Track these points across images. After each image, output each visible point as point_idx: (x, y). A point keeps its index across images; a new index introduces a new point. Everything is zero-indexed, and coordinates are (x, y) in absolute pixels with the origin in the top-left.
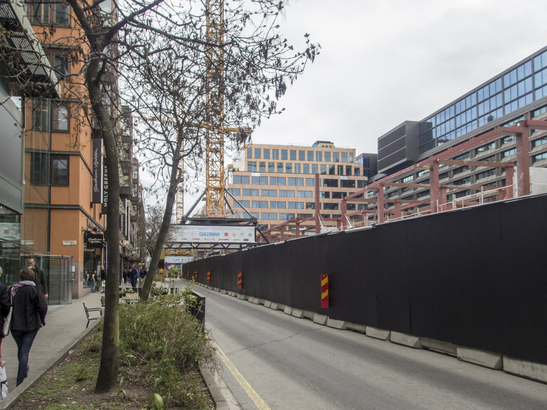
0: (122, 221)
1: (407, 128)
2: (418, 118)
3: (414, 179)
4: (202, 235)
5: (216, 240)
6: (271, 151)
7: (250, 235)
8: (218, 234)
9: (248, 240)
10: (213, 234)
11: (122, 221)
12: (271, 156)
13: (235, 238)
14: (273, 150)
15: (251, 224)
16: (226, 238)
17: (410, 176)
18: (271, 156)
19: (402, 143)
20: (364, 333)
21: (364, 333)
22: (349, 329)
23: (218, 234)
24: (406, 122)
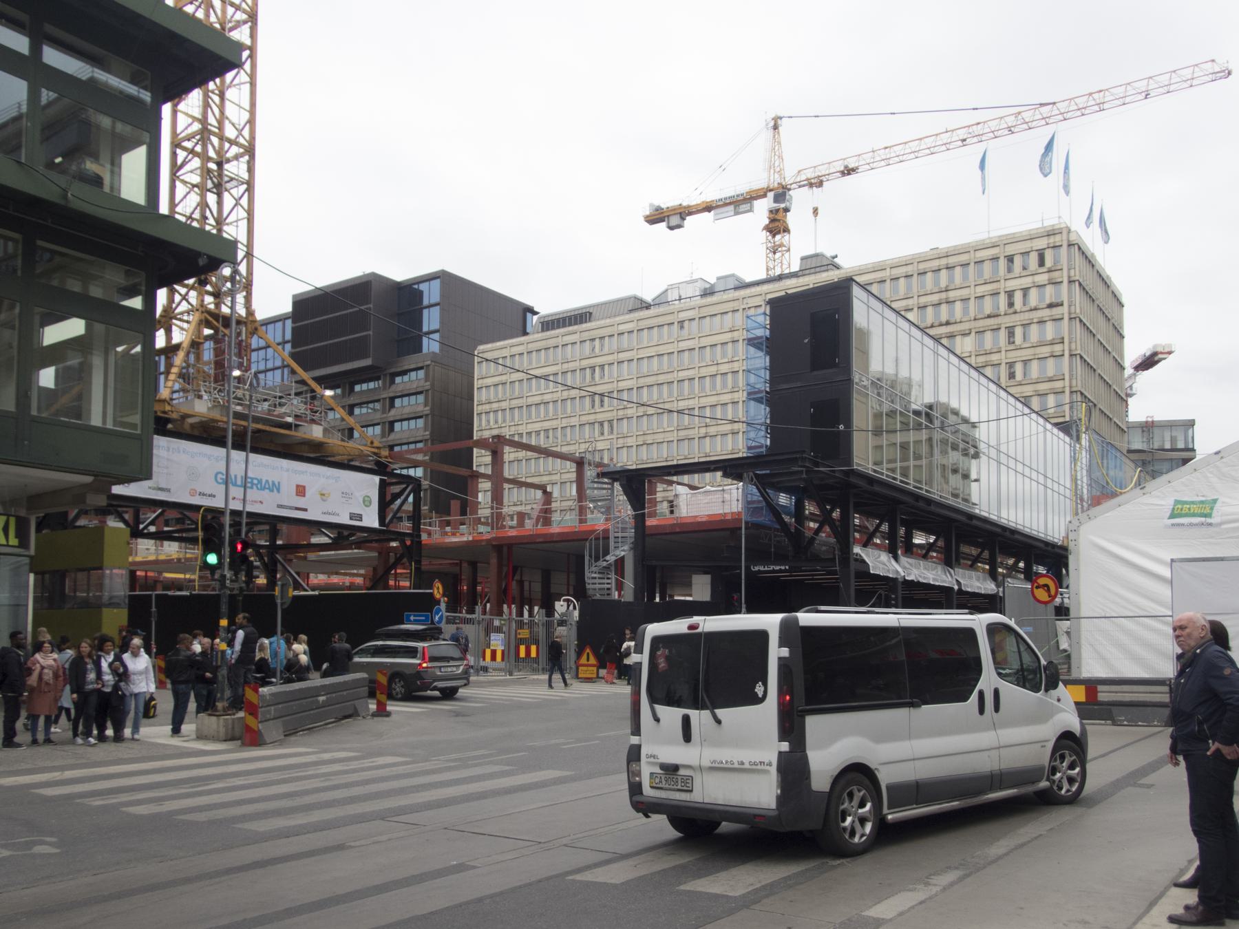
2: (399, 273)
7: (367, 502)
9: (359, 517)
16: (300, 502)
23: (275, 487)
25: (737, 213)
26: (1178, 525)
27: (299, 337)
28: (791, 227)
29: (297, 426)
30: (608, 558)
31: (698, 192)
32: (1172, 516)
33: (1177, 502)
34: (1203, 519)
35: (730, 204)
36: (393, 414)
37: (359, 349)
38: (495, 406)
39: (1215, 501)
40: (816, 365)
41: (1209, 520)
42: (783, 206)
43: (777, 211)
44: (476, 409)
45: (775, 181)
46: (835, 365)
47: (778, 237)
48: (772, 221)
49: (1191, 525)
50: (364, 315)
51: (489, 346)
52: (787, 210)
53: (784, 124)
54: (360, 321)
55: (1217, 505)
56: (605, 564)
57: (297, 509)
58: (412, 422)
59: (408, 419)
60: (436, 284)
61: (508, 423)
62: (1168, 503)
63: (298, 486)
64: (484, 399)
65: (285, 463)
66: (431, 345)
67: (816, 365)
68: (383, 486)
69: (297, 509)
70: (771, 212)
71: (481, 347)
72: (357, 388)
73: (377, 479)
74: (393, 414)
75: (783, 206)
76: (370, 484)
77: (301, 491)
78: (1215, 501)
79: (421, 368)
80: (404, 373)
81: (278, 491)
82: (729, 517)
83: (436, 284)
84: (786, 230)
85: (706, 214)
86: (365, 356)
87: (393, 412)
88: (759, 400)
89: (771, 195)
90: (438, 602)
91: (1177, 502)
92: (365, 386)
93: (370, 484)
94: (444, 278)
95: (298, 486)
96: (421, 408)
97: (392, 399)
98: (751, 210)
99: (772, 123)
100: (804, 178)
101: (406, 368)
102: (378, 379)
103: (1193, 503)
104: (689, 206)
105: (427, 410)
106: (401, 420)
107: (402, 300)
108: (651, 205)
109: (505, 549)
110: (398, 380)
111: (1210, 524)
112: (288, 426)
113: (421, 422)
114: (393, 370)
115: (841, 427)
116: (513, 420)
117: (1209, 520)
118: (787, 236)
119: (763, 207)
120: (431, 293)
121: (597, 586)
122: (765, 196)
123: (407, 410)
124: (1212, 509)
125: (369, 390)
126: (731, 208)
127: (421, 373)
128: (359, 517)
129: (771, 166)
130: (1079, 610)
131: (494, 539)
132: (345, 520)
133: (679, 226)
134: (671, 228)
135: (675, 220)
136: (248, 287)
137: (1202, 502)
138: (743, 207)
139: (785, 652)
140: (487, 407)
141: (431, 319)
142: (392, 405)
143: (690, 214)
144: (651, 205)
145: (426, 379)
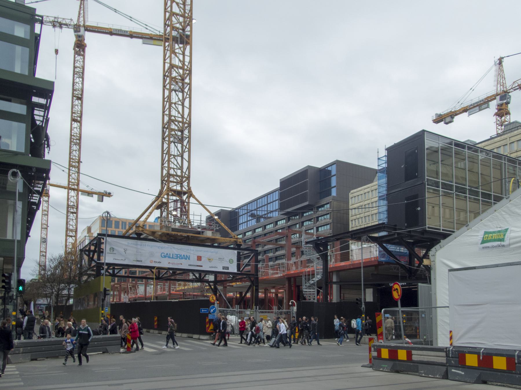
0: (13, 380)
1: (309, 172)
2: (320, 164)
3: (252, 234)
4: (165, 257)
5: (185, 265)
6: (121, 223)
7: (231, 261)
8: (187, 258)
9: (228, 268)
10: (178, 257)
11: (13, 380)
12: (120, 227)
13: (211, 264)
14: (122, 222)
15: (232, 246)
16: (199, 263)
17: (250, 231)
18: (120, 227)
19: (304, 186)
20: (192, 338)
21: (192, 338)
22: (189, 337)
23: (187, 258)
24: (309, 166)
25: (480, 110)
26: (486, 247)
27: (282, 196)
28: (511, 112)
29: (203, 232)
30: (314, 279)
31: (460, 103)
32: (483, 242)
33: (486, 233)
34: (499, 243)
35: (477, 106)
36: (318, 224)
37: (303, 198)
38: (358, 216)
39: (506, 230)
40: (407, 178)
41: (503, 243)
42: (505, 101)
43: (502, 105)
44: (351, 219)
45: (500, 89)
46: (416, 177)
47: (503, 118)
48: (499, 110)
49: (493, 247)
50: (305, 183)
51: (355, 190)
52: (507, 103)
53: (505, 61)
54: (304, 186)
55: (508, 234)
56: (312, 282)
57: (198, 266)
58: (325, 227)
59: (324, 226)
60: (334, 167)
61: (364, 223)
62: (480, 235)
63: (198, 257)
64: (353, 214)
65: (192, 247)
66: (334, 192)
67: (407, 178)
68: (239, 253)
69: (198, 266)
70: (498, 106)
71: (352, 191)
72: (305, 215)
73: (236, 252)
74: (318, 224)
75: (505, 101)
76: (233, 254)
77: (199, 258)
78: (506, 230)
79: (328, 203)
80: (323, 206)
81: (189, 259)
82: (373, 259)
83: (334, 167)
84: (508, 113)
85: (465, 113)
86: (306, 201)
87: (318, 223)
88: (383, 199)
89: (498, 98)
90: (214, 304)
91: (486, 233)
92: (307, 214)
93: (233, 254)
94: (338, 163)
95: (201, 257)
96: (328, 220)
97: (318, 218)
98: (488, 107)
99: (498, 62)
100: (516, 85)
101: (322, 204)
102: (312, 210)
103: (494, 232)
104: (455, 111)
105: (331, 221)
106: (321, 226)
107: (323, 174)
108: (436, 114)
109: (292, 279)
110: (320, 209)
111: (503, 246)
112: (199, 233)
113: (328, 226)
114: (317, 206)
115: (419, 209)
116: (373, 220)
117: (503, 243)
118: (508, 117)
119: (494, 104)
120: (334, 170)
121: (308, 293)
122: (495, 99)
123: (323, 222)
124: (504, 235)
125: (309, 215)
126: (478, 108)
127: (328, 206)
128: (228, 268)
129: (498, 82)
130: (436, 304)
131: (286, 275)
132: (220, 269)
133: (451, 122)
134: (447, 123)
135: (448, 120)
136: (188, 178)
137: (499, 232)
138: (483, 106)
139: (22, 337)
140: (355, 217)
141: (334, 181)
142: (318, 220)
143: (456, 115)
144: (436, 114)
145: (330, 208)
